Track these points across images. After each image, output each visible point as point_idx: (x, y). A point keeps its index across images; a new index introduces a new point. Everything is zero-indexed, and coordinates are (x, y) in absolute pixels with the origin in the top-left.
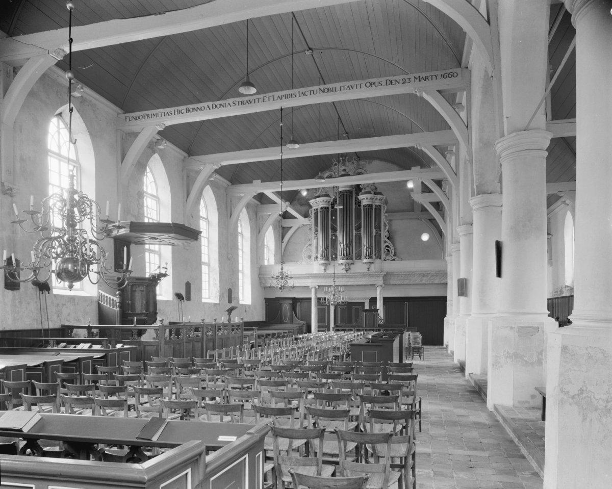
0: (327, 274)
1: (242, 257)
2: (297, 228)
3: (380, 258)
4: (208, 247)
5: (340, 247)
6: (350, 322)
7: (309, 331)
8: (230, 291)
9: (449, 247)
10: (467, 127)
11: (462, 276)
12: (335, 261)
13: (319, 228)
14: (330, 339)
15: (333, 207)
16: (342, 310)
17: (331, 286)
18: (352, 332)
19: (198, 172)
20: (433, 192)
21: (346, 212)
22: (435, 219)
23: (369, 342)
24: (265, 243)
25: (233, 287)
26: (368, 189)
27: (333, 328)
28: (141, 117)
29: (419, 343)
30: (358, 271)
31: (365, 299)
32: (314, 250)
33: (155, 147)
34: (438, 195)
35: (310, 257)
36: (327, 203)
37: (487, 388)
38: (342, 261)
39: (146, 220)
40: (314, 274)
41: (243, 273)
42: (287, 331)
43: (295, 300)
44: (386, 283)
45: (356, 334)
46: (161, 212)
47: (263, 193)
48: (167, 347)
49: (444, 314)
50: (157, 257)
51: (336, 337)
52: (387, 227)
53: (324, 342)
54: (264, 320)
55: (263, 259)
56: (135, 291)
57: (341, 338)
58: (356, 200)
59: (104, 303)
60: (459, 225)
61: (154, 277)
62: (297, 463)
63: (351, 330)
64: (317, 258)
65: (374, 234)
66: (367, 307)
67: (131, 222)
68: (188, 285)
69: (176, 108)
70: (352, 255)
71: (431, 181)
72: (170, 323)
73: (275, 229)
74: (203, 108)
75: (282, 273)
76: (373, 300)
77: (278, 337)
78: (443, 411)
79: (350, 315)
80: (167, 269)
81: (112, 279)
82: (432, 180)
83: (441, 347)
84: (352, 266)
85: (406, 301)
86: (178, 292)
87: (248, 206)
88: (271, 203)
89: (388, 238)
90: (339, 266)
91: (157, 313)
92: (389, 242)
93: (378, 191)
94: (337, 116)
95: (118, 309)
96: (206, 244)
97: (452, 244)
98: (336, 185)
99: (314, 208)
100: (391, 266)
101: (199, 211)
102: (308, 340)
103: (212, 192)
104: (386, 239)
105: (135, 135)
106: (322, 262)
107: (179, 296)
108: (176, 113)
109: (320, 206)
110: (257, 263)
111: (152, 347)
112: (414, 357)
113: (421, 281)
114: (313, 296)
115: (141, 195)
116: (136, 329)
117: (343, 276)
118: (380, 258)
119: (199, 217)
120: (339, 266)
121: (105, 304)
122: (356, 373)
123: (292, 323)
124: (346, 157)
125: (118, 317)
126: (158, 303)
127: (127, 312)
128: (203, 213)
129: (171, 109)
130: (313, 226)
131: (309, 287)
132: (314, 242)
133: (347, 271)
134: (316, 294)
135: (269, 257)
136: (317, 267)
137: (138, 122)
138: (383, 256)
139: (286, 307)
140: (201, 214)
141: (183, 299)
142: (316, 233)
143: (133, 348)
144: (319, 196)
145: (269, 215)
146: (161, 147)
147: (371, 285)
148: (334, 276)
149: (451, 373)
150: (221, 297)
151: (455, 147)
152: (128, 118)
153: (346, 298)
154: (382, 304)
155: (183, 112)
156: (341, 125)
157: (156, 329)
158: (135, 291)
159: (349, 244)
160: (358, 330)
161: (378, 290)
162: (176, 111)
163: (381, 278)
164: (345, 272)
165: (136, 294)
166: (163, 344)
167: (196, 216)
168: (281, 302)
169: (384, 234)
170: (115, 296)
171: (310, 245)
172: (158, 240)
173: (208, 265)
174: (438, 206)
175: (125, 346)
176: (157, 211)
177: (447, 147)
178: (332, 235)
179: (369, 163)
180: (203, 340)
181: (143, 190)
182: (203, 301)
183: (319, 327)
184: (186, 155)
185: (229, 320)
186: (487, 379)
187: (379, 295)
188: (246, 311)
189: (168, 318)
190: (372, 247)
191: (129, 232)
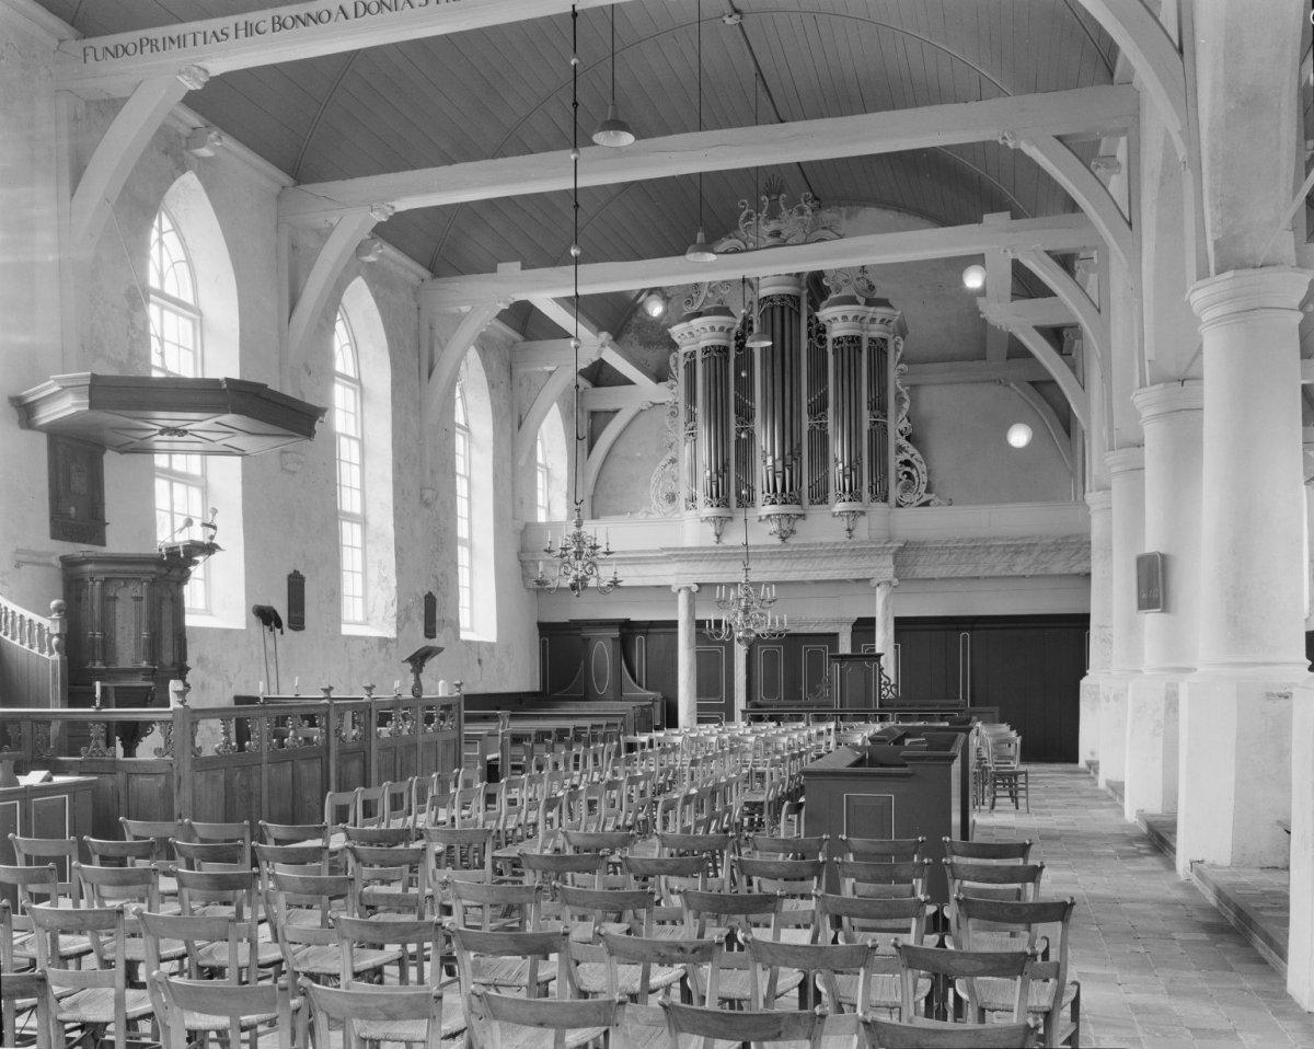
0: (727, 548)
1: (469, 499)
2: (633, 412)
3: (885, 500)
4: (362, 466)
5: (764, 466)
6: (793, 692)
7: (671, 720)
8: (430, 603)
9: (1100, 459)
10: (1181, 51)
11: (1151, 546)
12: (750, 510)
13: (699, 410)
14: (735, 747)
15: (740, 347)
16: (771, 657)
17: (736, 584)
18: (802, 724)
19: (323, 235)
20: (1051, 294)
21: (781, 358)
22: (1053, 382)
23: (859, 762)
24: (540, 459)
25: (438, 589)
26: (847, 291)
27: (743, 711)
28: (131, 49)
29: (1012, 758)
30: (818, 540)
31: (840, 622)
32: (685, 476)
33: (186, 154)
34: (1068, 302)
35: (672, 498)
36: (850, 323)
37: (1285, 922)
38: (770, 509)
39: (156, 374)
40: (683, 549)
41: (471, 549)
42: (603, 722)
43: (628, 628)
44: (902, 576)
45: (814, 732)
46: (208, 356)
47: (527, 301)
48: (201, 778)
49: (1080, 667)
50: (195, 494)
51: (752, 739)
52: (906, 406)
53: (715, 757)
54: (538, 689)
55: (533, 506)
56: (115, 598)
57: (767, 744)
58: (810, 325)
59: (13, 638)
60: (1142, 385)
61: (172, 552)
62: (684, 935)
63: (799, 718)
64: (693, 499)
65: (866, 426)
66: (845, 648)
67: (94, 377)
68: (296, 584)
69: (241, 19)
70: (799, 489)
71: (1046, 256)
72: (239, 700)
73: (566, 416)
74: (325, 16)
75: (578, 538)
76: (864, 627)
77: (578, 739)
78: (1136, 1009)
79: (795, 671)
80: (215, 528)
81: (41, 560)
82: (1048, 252)
83: (1070, 766)
84: (799, 525)
85: (964, 630)
86: (265, 604)
87: (484, 344)
88: (556, 338)
89: (908, 439)
90: (761, 522)
91: (188, 669)
92: (912, 450)
93: (876, 296)
94: (752, 64)
95: (56, 656)
96: (356, 459)
97: (1112, 449)
98: (750, 273)
99: (684, 349)
100: (914, 522)
101: (329, 356)
102: (663, 751)
103: (372, 300)
104: (903, 441)
105: (110, 106)
106: (709, 511)
107: (266, 616)
108: (242, 33)
109: (704, 344)
110: (514, 518)
111: (152, 779)
112: (997, 800)
113: (1010, 567)
114: (682, 616)
115: (137, 297)
116: (98, 722)
117: (773, 555)
118: (885, 500)
119: (327, 374)
120: (761, 522)
121: (17, 642)
122: (847, 941)
123: (619, 696)
124: (779, 194)
125: (55, 683)
126: (188, 635)
127: (89, 666)
128: (343, 362)
129: (228, 22)
130: (682, 407)
131: (668, 587)
132: (686, 451)
133: (783, 539)
134: (691, 608)
135: (551, 503)
136: (693, 526)
137: (121, 64)
138: (894, 492)
139: (604, 648)
140: (339, 366)
141: (279, 624)
142: (691, 425)
143: (76, 784)
144: (699, 314)
145: (551, 373)
146: (205, 152)
147: (857, 581)
148: (747, 555)
149: (1125, 856)
150: (402, 619)
151: (1123, 140)
152: (90, 52)
153: (781, 622)
154: (892, 639)
155: (261, 29)
156: (763, 97)
157: (167, 722)
158: (115, 598)
159: (790, 456)
160: (820, 719)
161: (880, 595)
162: (242, 26)
163: (889, 560)
164: (779, 542)
165: (119, 610)
166: (188, 767)
167: (324, 372)
168: (586, 633)
169: (896, 424)
170: (46, 614)
171: (673, 461)
172: (186, 438)
173: (363, 520)
174: (1059, 336)
175: (58, 779)
176: (195, 353)
177: (1097, 143)
178: (739, 431)
179: (848, 218)
180: (328, 754)
181: (145, 280)
182: (346, 630)
183: (700, 707)
184: (285, 179)
185: (417, 688)
186: (1287, 886)
187: (883, 612)
188: (480, 661)
189: (230, 685)
190: (861, 465)
191: (87, 408)
